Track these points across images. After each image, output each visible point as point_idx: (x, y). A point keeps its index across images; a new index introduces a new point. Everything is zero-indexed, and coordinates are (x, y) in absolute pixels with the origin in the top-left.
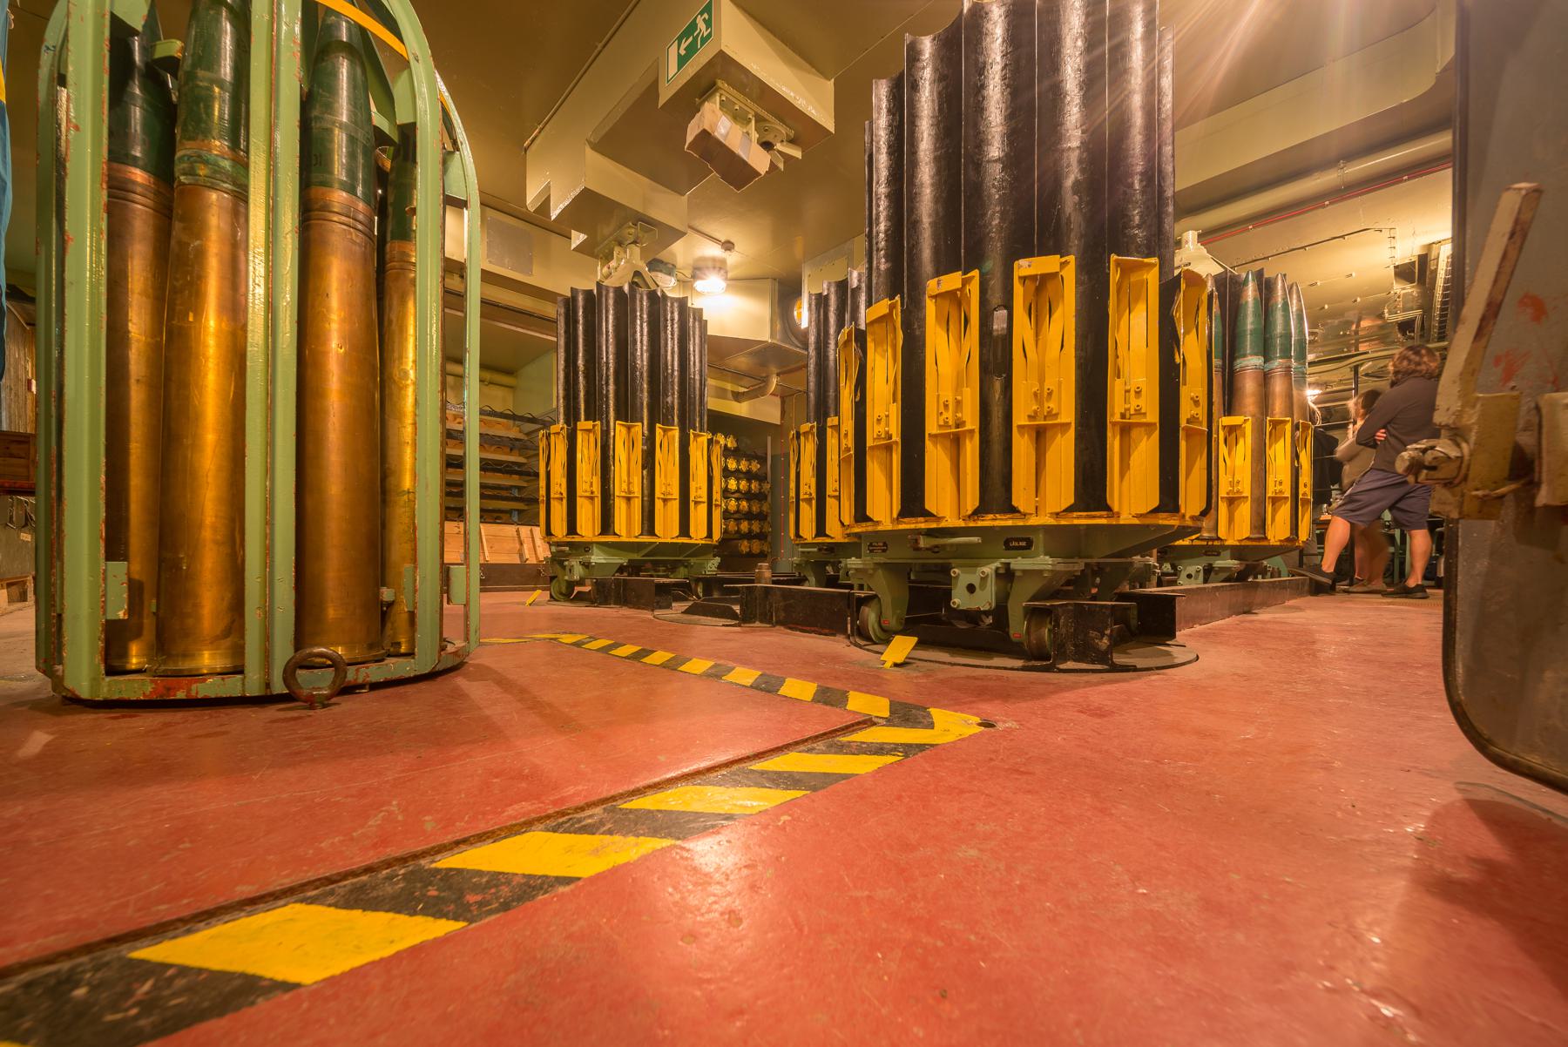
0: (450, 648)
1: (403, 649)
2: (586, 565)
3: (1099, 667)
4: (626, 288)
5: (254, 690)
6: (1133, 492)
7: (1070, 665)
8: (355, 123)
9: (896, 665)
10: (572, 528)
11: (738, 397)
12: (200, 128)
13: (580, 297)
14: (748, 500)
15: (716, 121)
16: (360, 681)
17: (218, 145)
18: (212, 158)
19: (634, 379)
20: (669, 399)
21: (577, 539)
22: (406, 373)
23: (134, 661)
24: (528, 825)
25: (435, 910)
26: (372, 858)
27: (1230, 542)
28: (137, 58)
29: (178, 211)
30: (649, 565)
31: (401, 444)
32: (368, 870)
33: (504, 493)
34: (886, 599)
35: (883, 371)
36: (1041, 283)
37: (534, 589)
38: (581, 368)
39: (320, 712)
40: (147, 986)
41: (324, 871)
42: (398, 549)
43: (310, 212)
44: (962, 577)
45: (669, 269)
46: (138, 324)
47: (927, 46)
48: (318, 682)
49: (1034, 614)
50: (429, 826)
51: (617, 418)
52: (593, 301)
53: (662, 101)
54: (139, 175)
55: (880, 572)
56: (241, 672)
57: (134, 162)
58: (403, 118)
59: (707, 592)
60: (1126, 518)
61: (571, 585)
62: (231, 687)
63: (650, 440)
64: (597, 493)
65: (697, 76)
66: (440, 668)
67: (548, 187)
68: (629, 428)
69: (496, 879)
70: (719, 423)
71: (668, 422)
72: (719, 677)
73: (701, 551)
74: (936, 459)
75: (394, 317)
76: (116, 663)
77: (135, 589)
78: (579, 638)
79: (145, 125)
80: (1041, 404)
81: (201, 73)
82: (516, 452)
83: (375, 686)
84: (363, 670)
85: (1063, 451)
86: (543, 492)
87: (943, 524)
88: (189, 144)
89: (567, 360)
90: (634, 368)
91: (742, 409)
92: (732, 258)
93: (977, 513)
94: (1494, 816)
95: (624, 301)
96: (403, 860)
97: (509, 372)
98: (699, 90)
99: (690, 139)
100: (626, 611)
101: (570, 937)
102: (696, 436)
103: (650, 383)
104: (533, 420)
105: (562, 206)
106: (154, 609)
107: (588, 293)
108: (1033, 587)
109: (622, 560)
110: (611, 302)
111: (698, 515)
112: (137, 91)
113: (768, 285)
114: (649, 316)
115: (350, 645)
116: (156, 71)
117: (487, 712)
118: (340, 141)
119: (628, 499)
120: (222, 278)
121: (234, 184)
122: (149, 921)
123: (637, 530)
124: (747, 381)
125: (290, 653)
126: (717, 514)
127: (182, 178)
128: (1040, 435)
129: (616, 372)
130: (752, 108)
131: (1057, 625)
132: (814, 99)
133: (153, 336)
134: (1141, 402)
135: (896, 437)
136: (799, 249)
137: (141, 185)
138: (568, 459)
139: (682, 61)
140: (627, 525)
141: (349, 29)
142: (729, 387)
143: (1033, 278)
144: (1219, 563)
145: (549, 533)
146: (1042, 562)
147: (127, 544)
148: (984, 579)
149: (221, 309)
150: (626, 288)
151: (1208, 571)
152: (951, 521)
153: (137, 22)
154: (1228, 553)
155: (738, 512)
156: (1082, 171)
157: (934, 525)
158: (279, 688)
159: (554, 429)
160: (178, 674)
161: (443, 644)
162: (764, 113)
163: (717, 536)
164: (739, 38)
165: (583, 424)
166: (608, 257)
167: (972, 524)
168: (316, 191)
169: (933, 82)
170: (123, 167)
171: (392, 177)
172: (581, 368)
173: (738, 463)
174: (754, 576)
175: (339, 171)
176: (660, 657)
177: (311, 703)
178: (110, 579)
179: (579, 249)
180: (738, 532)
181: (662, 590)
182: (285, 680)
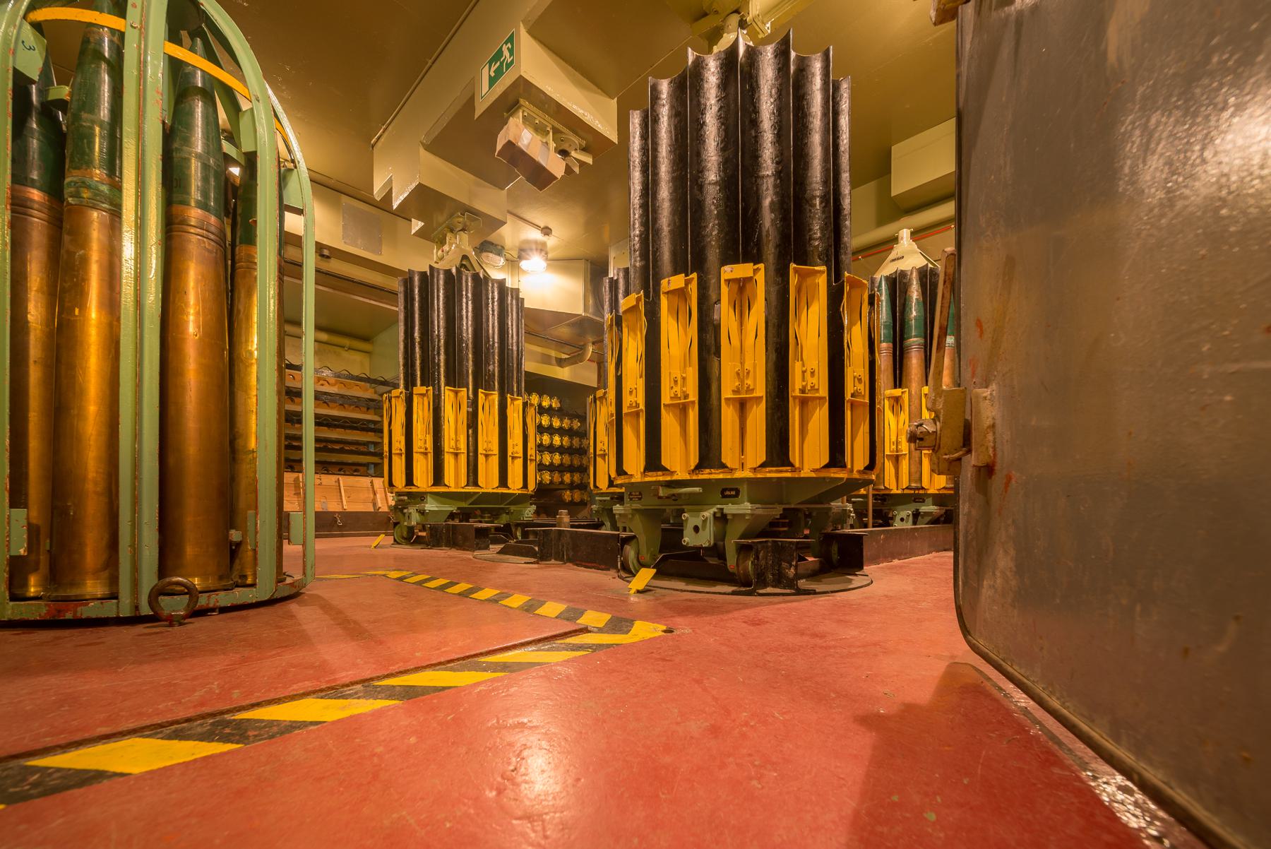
0: (289, 580)
1: (249, 581)
2: (422, 512)
3: (788, 591)
4: (454, 271)
5: (126, 612)
6: (810, 452)
7: (769, 590)
8: (208, 153)
9: (638, 592)
10: (409, 481)
11: (560, 363)
12: (84, 160)
13: (416, 278)
14: (570, 454)
15: (520, 133)
16: (211, 605)
17: (98, 173)
18: (93, 184)
19: (461, 350)
20: (491, 368)
21: (414, 490)
22: (251, 353)
23: (32, 590)
24: (306, 695)
25: (225, 739)
26: (191, 713)
27: (931, 491)
28: (34, 98)
29: (66, 226)
30: (478, 512)
31: (248, 412)
32: (188, 720)
33: (362, 448)
34: (642, 539)
35: (634, 347)
36: (742, 286)
37: (378, 535)
38: (417, 339)
39: (176, 628)
40: (36, 777)
41: (157, 720)
42: (243, 500)
43: (172, 225)
44: (690, 519)
45: (499, 250)
46: (35, 312)
47: (665, 87)
48: (175, 605)
49: (743, 549)
50: (235, 696)
51: (447, 384)
52: (427, 280)
53: (478, 113)
54: (36, 195)
55: (637, 516)
56: (116, 598)
57: (33, 184)
58: (247, 147)
59: (525, 534)
60: (806, 473)
61: (411, 530)
62: (109, 609)
63: (474, 403)
64: (430, 449)
65: (505, 94)
66: (277, 596)
67: (390, 181)
68: (456, 393)
69: (271, 723)
70: (537, 384)
71: (489, 387)
72: (496, 601)
73: (519, 500)
74: (669, 422)
75: (241, 308)
76: (18, 592)
77: (33, 531)
78: (405, 573)
79: (41, 153)
80: (742, 382)
81: (84, 115)
82: (372, 411)
83: (224, 610)
84: (214, 596)
85: (758, 416)
86: (386, 448)
87: (675, 477)
88: (76, 172)
89: (406, 332)
90: (461, 340)
91: (564, 374)
92: (551, 241)
93: (699, 467)
94: (976, 691)
95: (452, 281)
96: (213, 715)
97: (366, 339)
98: (507, 105)
99: (499, 147)
100: (454, 553)
101: (306, 750)
102: (513, 400)
103: (474, 354)
104: (385, 383)
105: (402, 198)
106: (48, 548)
107: (423, 275)
108: (740, 528)
109: (451, 508)
110: (441, 282)
111: (515, 469)
112: (35, 126)
113: (581, 265)
114: (473, 295)
115: (204, 576)
116: (49, 110)
117: (305, 627)
118: (195, 168)
119: (456, 455)
120: (101, 280)
121: (111, 204)
122: (39, 746)
123: (463, 481)
124: (567, 349)
125: (155, 581)
126: (532, 468)
127: (70, 200)
128: (742, 406)
129: (446, 343)
130: (549, 122)
131: (757, 558)
132: (598, 114)
133: (47, 326)
134: (815, 380)
135: (642, 407)
136: (606, 236)
137: (38, 202)
138: (408, 419)
139: (492, 81)
140: (455, 477)
141: (203, 77)
142: (553, 353)
143: (737, 281)
144: (924, 509)
145: (391, 484)
146: (744, 507)
147: (27, 495)
148: (705, 521)
149: (101, 305)
150: (454, 271)
151: (916, 515)
152: (681, 475)
153: (34, 74)
154: (930, 500)
155: (561, 465)
156: (776, 193)
157: (668, 478)
158: (146, 610)
159: (395, 393)
160: (67, 599)
161: (280, 577)
162: (560, 127)
163: (532, 486)
164: (534, 63)
165: (419, 389)
166: (442, 242)
167: (695, 477)
168: (176, 209)
169: (670, 118)
170: (23, 188)
171: (240, 192)
172: (417, 339)
173: (562, 421)
174: (557, 522)
175: (195, 194)
176: (463, 587)
177: (171, 621)
178: (13, 522)
179: (420, 234)
180: (562, 482)
181: (481, 533)
182: (150, 603)
